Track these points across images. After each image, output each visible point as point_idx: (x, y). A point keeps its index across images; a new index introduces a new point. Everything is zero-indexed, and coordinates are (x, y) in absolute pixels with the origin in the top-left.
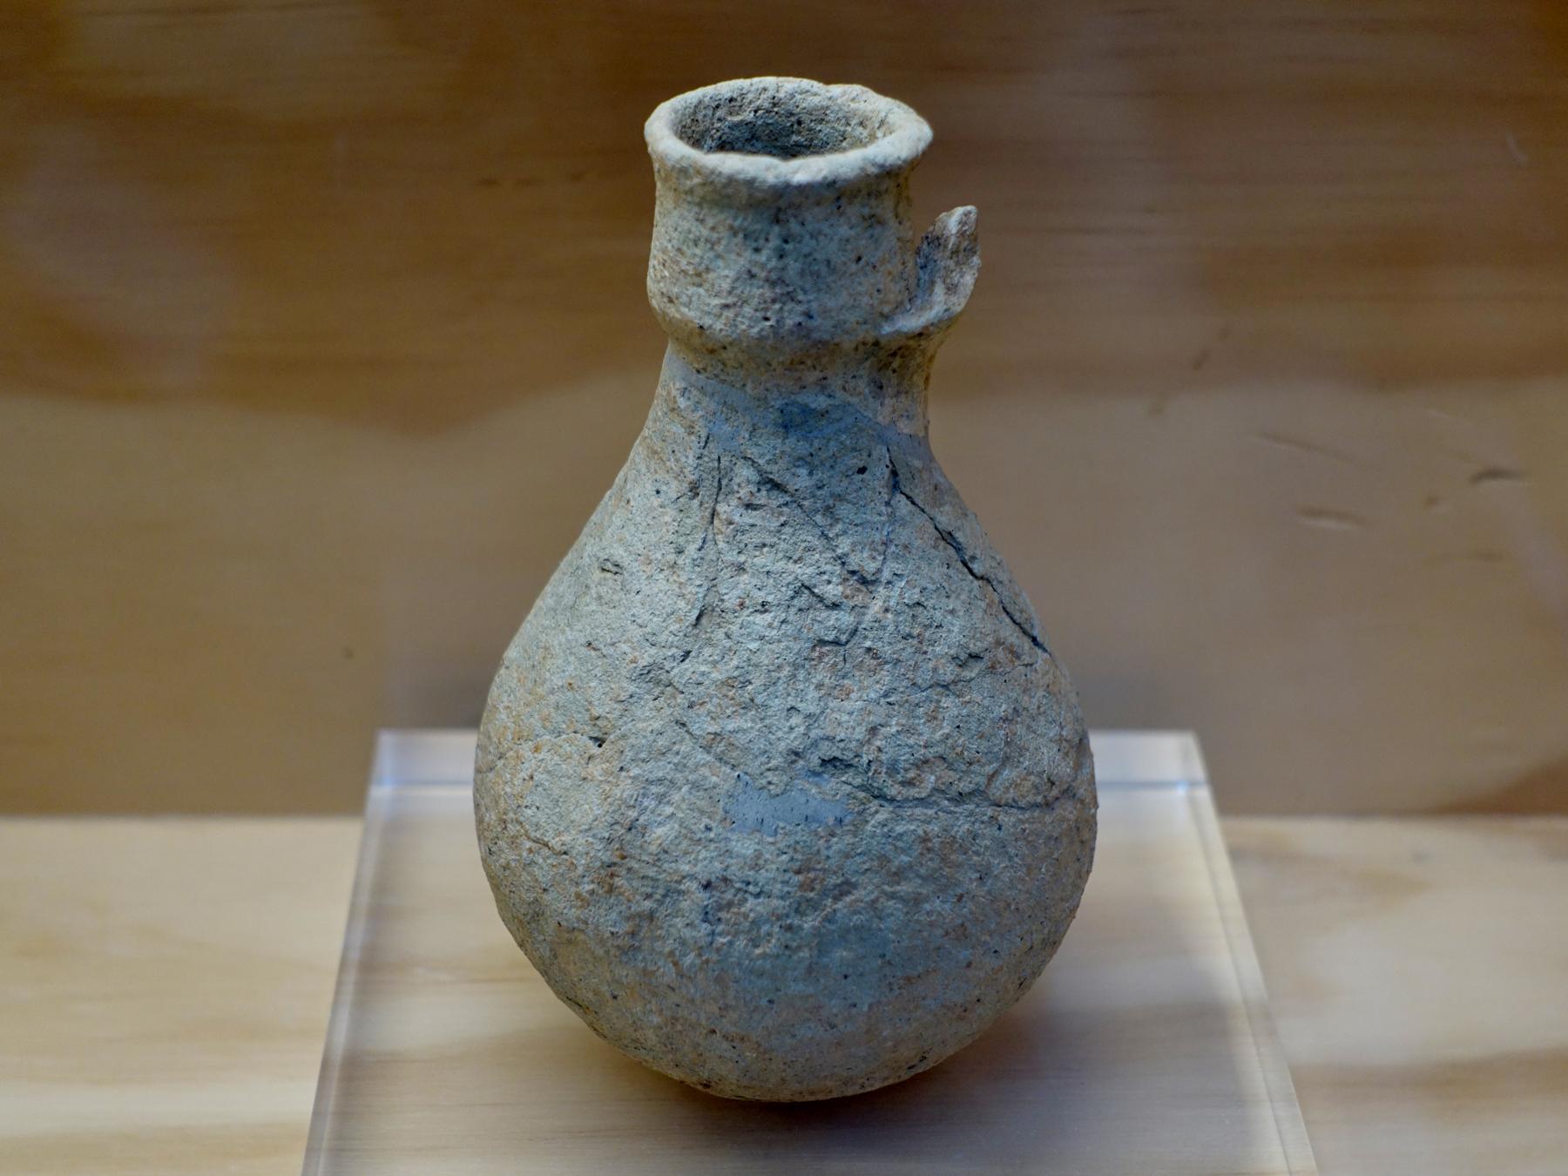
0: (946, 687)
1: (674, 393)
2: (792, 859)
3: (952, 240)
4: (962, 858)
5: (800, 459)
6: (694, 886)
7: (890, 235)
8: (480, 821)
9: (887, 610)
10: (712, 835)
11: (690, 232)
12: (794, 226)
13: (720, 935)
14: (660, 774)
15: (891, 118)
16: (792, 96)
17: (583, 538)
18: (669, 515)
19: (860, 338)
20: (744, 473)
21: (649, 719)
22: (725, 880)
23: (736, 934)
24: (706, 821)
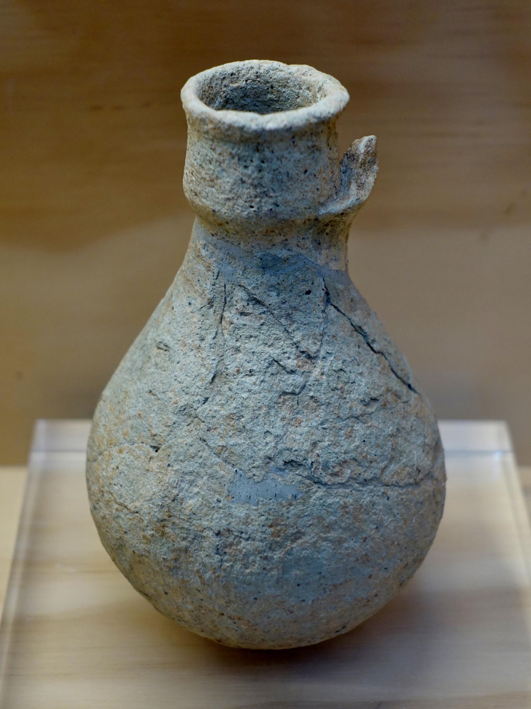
0: (357, 418)
1: (199, 246)
2: (267, 519)
3: (362, 157)
4: (366, 517)
5: (272, 286)
6: (211, 533)
7: (324, 158)
8: (89, 489)
9: (323, 374)
10: (221, 505)
11: (207, 155)
12: (268, 154)
13: (226, 561)
14: (191, 469)
15: (325, 87)
16: (268, 72)
17: (147, 327)
18: (197, 317)
19: (307, 217)
20: (240, 294)
21: (185, 437)
22: (229, 530)
23: (235, 561)
24: (217, 496)
